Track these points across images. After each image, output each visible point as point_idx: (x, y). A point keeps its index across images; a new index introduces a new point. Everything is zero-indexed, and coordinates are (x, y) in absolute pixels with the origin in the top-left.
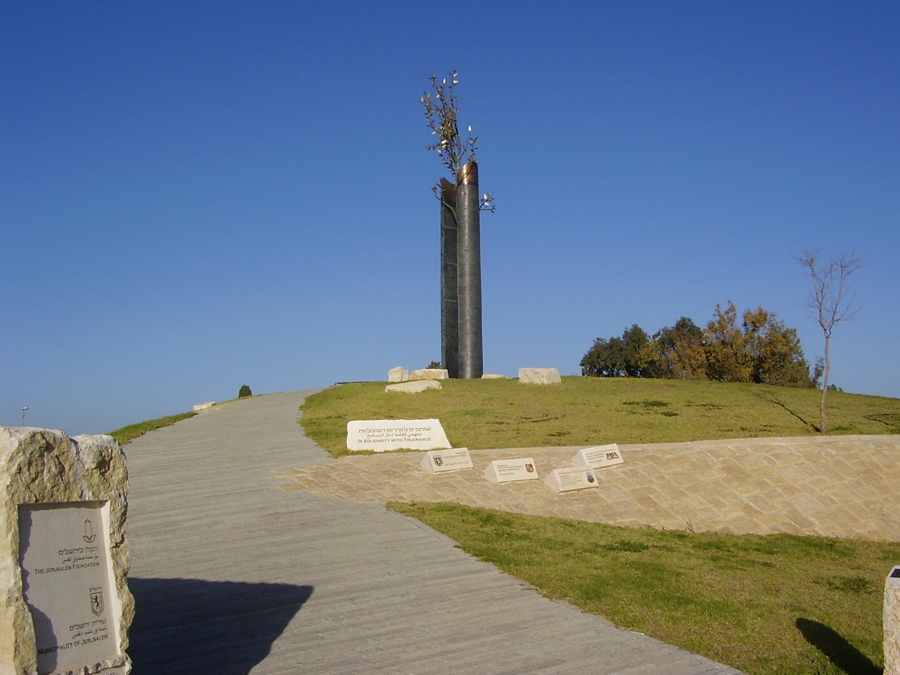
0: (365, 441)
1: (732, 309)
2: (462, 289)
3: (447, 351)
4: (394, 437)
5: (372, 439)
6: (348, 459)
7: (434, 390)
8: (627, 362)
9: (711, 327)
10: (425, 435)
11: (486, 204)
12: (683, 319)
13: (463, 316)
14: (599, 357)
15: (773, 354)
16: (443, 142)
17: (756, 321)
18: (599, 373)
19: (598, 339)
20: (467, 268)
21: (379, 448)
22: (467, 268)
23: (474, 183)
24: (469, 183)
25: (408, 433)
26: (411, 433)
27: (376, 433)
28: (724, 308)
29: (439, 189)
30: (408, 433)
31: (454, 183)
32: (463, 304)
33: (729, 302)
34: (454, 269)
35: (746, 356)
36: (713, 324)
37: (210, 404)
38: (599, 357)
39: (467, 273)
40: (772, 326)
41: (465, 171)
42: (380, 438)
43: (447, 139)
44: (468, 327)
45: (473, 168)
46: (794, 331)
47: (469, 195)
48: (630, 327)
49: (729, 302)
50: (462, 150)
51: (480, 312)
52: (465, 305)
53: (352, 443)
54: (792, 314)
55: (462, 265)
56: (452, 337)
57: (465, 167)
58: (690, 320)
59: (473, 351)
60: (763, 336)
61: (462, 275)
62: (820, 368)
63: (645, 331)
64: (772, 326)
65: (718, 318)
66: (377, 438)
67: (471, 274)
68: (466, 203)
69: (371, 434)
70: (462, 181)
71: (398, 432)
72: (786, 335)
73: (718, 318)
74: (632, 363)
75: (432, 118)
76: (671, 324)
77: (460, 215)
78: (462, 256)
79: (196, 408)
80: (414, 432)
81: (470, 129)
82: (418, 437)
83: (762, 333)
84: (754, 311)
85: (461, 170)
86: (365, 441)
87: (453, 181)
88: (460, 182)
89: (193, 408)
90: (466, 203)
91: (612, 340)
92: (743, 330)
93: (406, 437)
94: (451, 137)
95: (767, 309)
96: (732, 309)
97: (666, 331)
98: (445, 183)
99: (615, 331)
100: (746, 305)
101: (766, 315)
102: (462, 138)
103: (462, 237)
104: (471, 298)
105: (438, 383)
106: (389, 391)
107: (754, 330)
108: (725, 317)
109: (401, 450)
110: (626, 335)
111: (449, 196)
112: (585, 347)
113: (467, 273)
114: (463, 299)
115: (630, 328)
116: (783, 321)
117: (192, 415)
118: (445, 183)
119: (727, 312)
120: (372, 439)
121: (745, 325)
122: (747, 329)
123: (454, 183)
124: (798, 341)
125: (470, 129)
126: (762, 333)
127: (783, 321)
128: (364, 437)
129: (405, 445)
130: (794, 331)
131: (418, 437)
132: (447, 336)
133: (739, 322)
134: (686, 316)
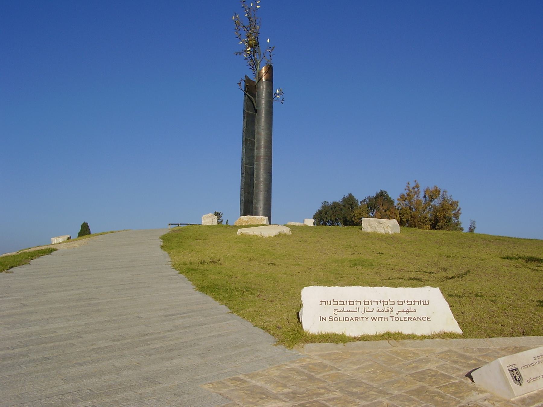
0: (331, 319)
1: (417, 186)
2: (258, 158)
3: (245, 204)
4: (375, 314)
5: (341, 315)
6: (311, 353)
7: (285, 235)
8: (345, 218)
9: (402, 197)
10: (422, 311)
11: (278, 96)
12: (382, 192)
13: (258, 178)
14: (326, 214)
15: (445, 217)
16: (248, 50)
17: (432, 195)
18: (325, 224)
19: (325, 202)
20: (263, 143)
21: (353, 330)
22: (263, 143)
23: (270, 80)
24: (267, 80)
25: (396, 308)
26: (400, 308)
27: (347, 307)
28: (412, 185)
29: (243, 83)
30: (396, 308)
31: (256, 80)
32: (258, 169)
33: (415, 181)
34: (253, 143)
35: (426, 218)
36: (404, 195)
37: (66, 237)
38: (326, 214)
39: (262, 146)
40: (444, 198)
41: (263, 71)
42: (354, 315)
43: (252, 47)
44: (262, 186)
45: (270, 70)
46: (456, 203)
47: (266, 89)
48: (347, 195)
49: (415, 181)
50: (262, 56)
51: (271, 176)
52: (260, 169)
53: (310, 324)
54: (454, 190)
55: (259, 140)
56: (249, 193)
57: (263, 68)
58: (386, 192)
59: (265, 204)
60: (437, 205)
61: (259, 148)
62: (473, 228)
63: (356, 198)
64: (444, 198)
65: (408, 191)
66: (350, 315)
67: (266, 147)
68: (264, 95)
69: (339, 308)
70: (261, 78)
71: (381, 307)
72: (454, 204)
73: (408, 191)
74: (348, 218)
75: (239, 32)
76: (373, 194)
77: (259, 103)
78: (259, 133)
79: (55, 241)
80: (405, 307)
81: (268, 41)
82: (411, 314)
83: (437, 203)
84: (432, 188)
85: (261, 70)
86: (331, 319)
87: (253, 78)
88: (260, 79)
89: (51, 241)
90: (264, 95)
91: (334, 203)
92: (423, 200)
93: (394, 314)
94: (255, 46)
95: (442, 187)
96: (417, 186)
97: (370, 199)
98: (247, 80)
99: (338, 198)
100: (426, 183)
101: (439, 191)
102: (262, 47)
103: (260, 119)
104: (265, 165)
105: (289, 229)
106: (242, 234)
107: (431, 201)
108: (412, 191)
109: (388, 336)
110: (344, 199)
111: (251, 90)
112: (318, 207)
113: (262, 146)
114: (259, 165)
115: (347, 195)
116: (451, 196)
117: (50, 251)
118: (247, 80)
119: (413, 188)
120: (341, 315)
121: (425, 197)
122: (426, 200)
123: (256, 80)
124: (460, 209)
125: (268, 41)
126: (437, 203)
127: (451, 196)
128: (328, 312)
129: (393, 327)
130: (456, 203)
131: (411, 314)
132: (245, 193)
133: (422, 195)
134: (383, 190)
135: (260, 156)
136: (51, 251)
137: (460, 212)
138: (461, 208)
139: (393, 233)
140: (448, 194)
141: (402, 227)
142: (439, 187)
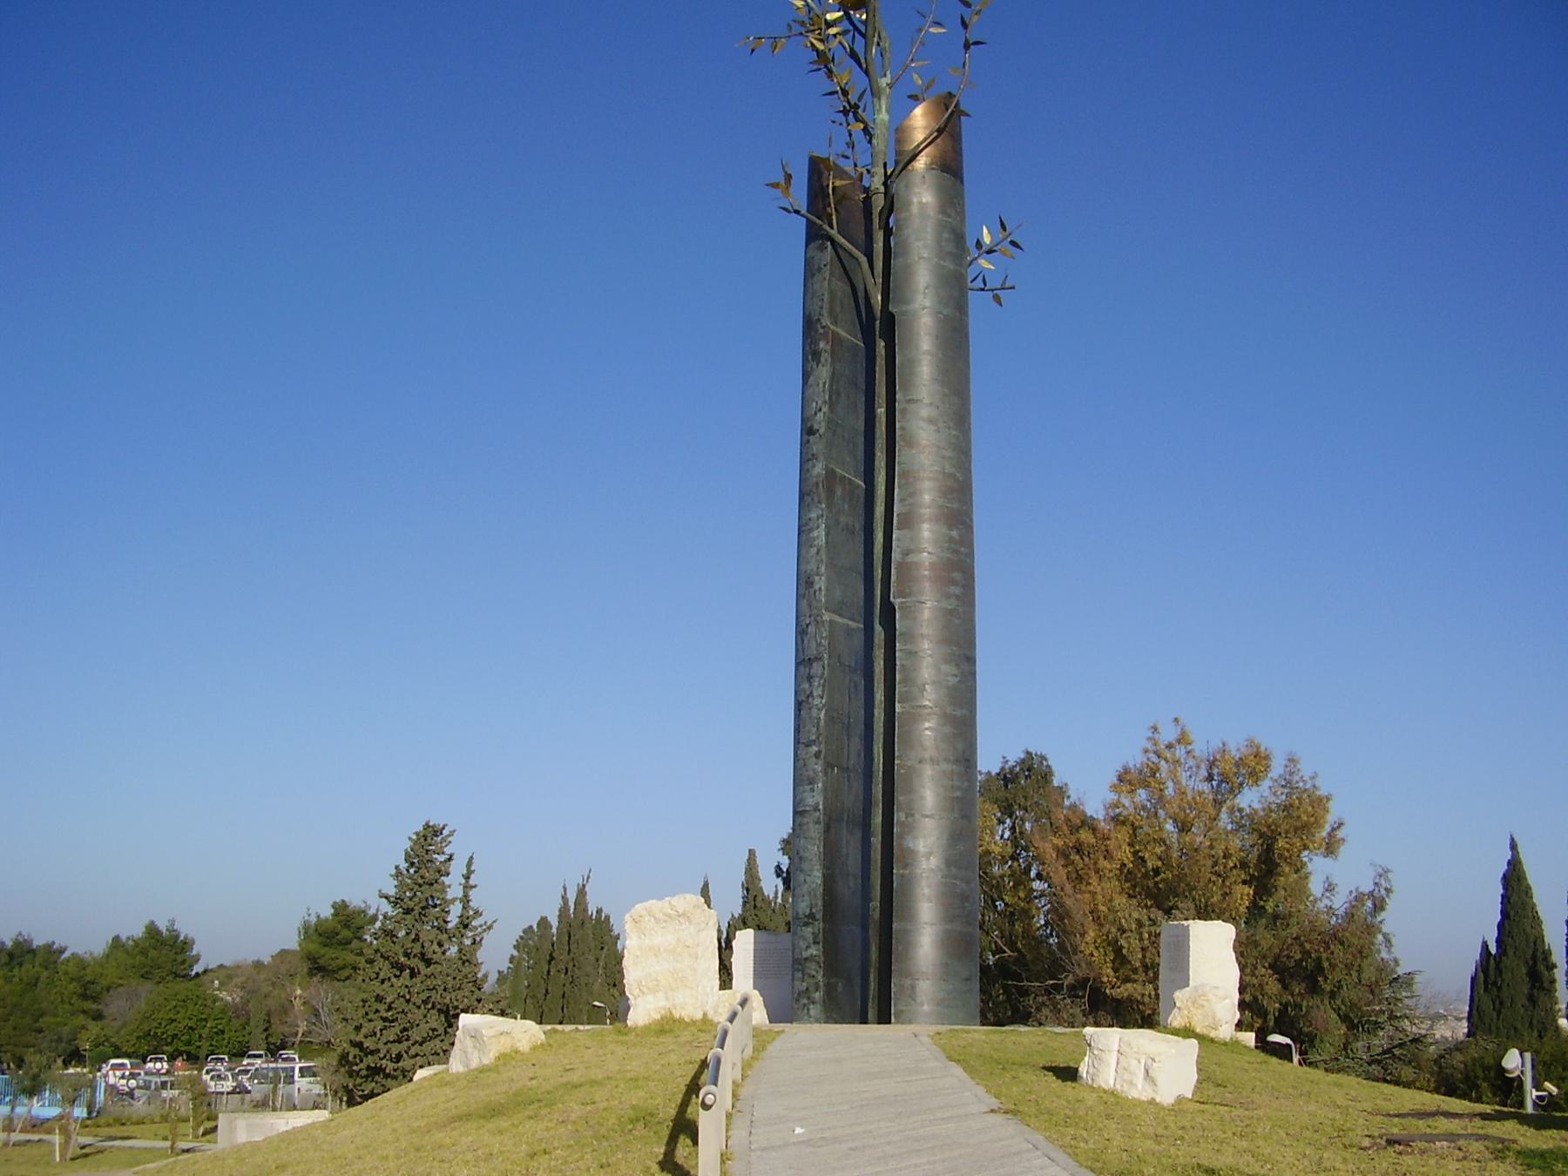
1: (1183, 739)
17: (1231, 774)
20: (929, 697)
22: (929, 697)
28: (1168, 734)
40: (1288, 784)
49: (1176, 720)
63: (634, 973)
83: (1251, 799)
84: (1236, 746)
96: (1183, 739)
100: (1218, 731)
119: (1169, 746)
135: (917, 565)
136: (963, 523)
137: (1340, 834)
138: (1346, 820)
139: (460, 1024)
140: (1305, 770)
141: (899, 1014)
142: (1265, 743)
